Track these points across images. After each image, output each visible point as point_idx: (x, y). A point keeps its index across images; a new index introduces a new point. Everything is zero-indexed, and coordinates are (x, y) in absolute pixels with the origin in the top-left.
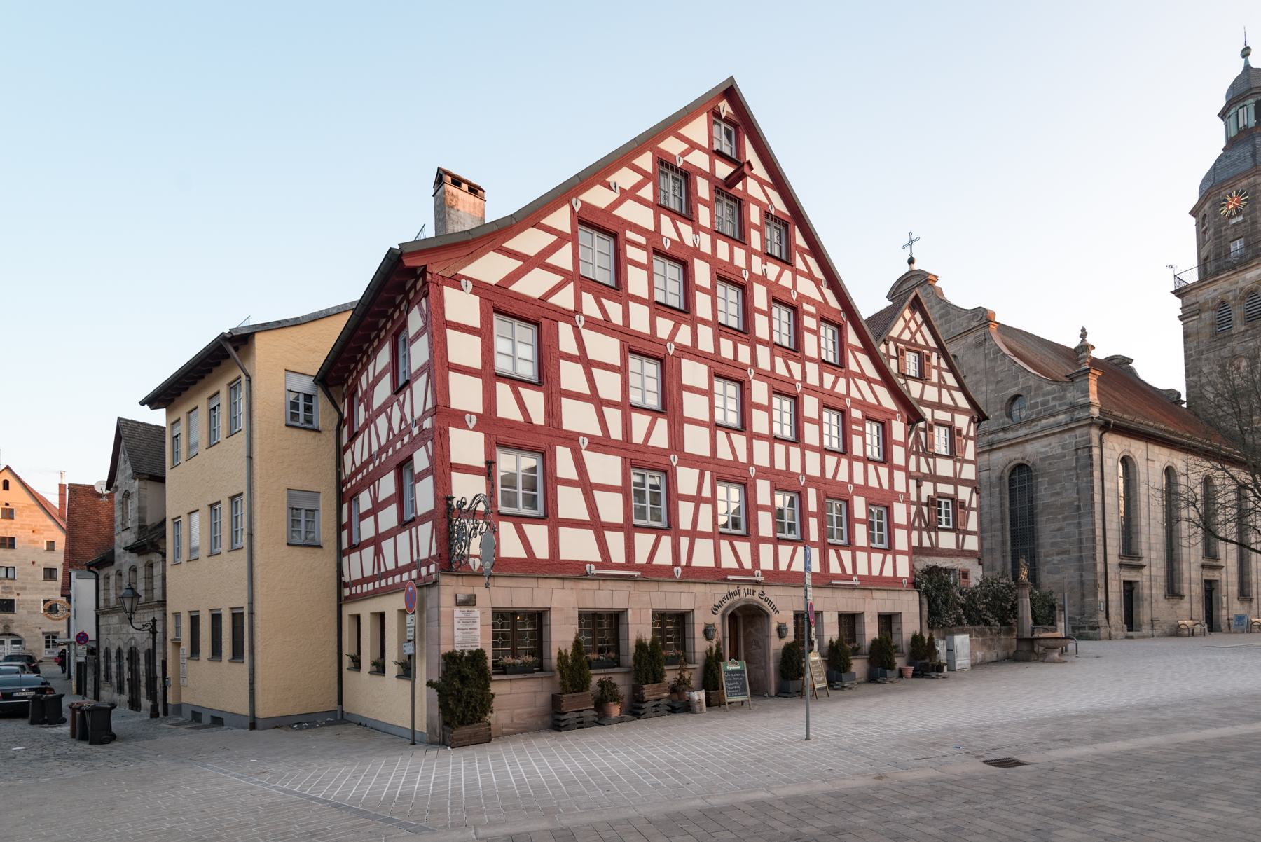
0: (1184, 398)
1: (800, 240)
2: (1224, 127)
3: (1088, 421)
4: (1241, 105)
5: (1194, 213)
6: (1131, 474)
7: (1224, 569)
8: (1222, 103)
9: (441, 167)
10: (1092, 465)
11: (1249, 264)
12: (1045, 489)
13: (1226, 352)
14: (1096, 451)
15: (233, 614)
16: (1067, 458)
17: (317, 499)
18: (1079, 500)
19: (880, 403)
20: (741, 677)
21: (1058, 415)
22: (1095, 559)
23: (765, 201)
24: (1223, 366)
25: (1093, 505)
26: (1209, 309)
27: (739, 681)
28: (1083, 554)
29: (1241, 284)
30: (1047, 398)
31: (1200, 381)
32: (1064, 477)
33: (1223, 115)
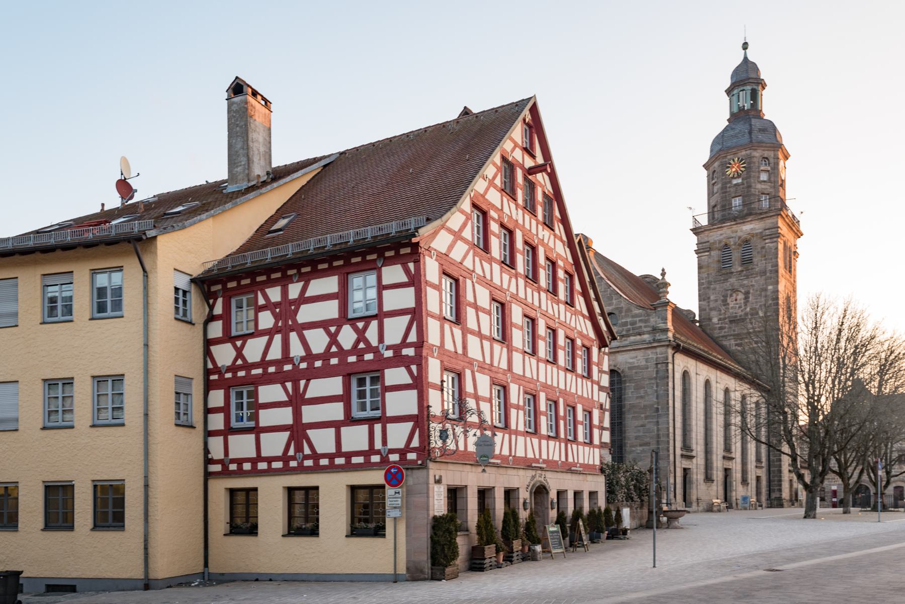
0: (697, 318)
1: (557, 213)
2: (728, 102)
3: (667, 343)
4: (742, 88)
5: (706, 166)
6: (687, 385)
7: (734, 461)
8: (727, 84)
9: (239, 76)
10: (668, 377)
11: (746, 219)
12: (632, 392)
13: (727, 285)
14: (670, 366)
15: (95, 486)
16: (649, 370)
17: (190, 385)
18: (658, 403)
19: (588, 335)
20: (557, 535)
21: (644, 334)
22: (668, 451)
23: (544, 184)
24: (725, 296)
25: (668, 408)
26: (716, 249)
27: (557, 538)
28: (660, 446)
29: (739, 234)
30: (635, 319)
31: (709, 305)
32: (647, 384)
33: (729, 92)
